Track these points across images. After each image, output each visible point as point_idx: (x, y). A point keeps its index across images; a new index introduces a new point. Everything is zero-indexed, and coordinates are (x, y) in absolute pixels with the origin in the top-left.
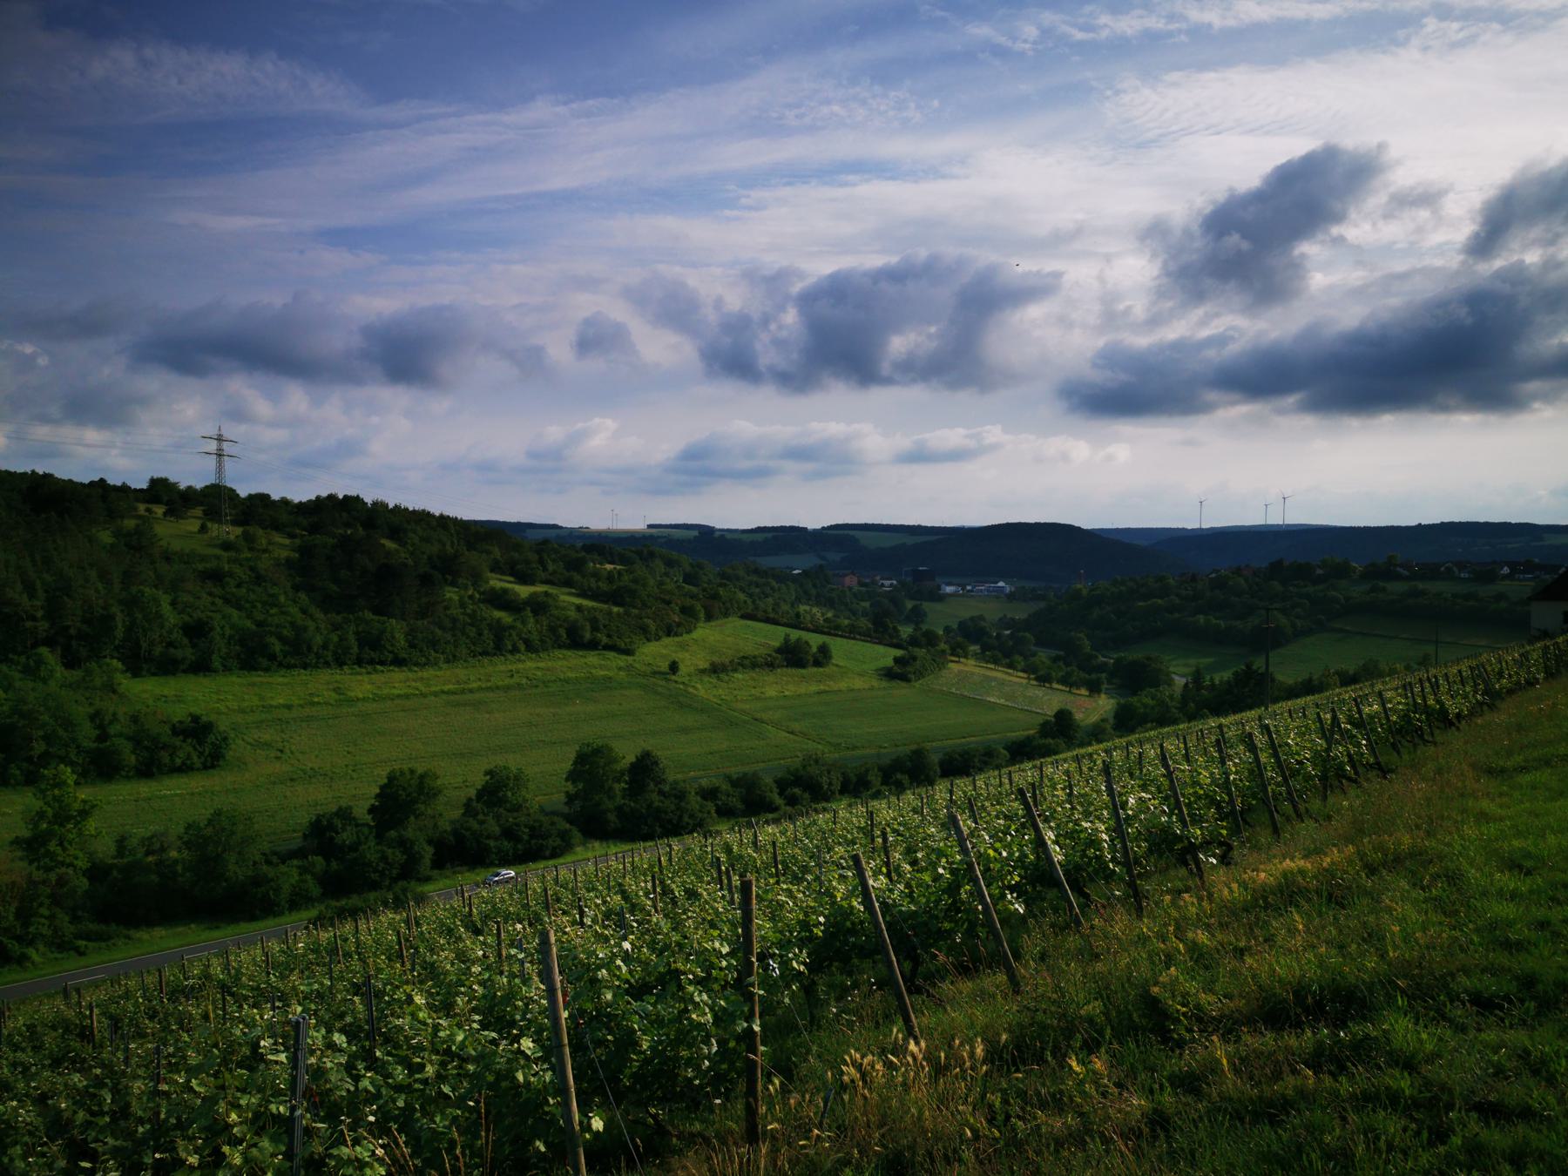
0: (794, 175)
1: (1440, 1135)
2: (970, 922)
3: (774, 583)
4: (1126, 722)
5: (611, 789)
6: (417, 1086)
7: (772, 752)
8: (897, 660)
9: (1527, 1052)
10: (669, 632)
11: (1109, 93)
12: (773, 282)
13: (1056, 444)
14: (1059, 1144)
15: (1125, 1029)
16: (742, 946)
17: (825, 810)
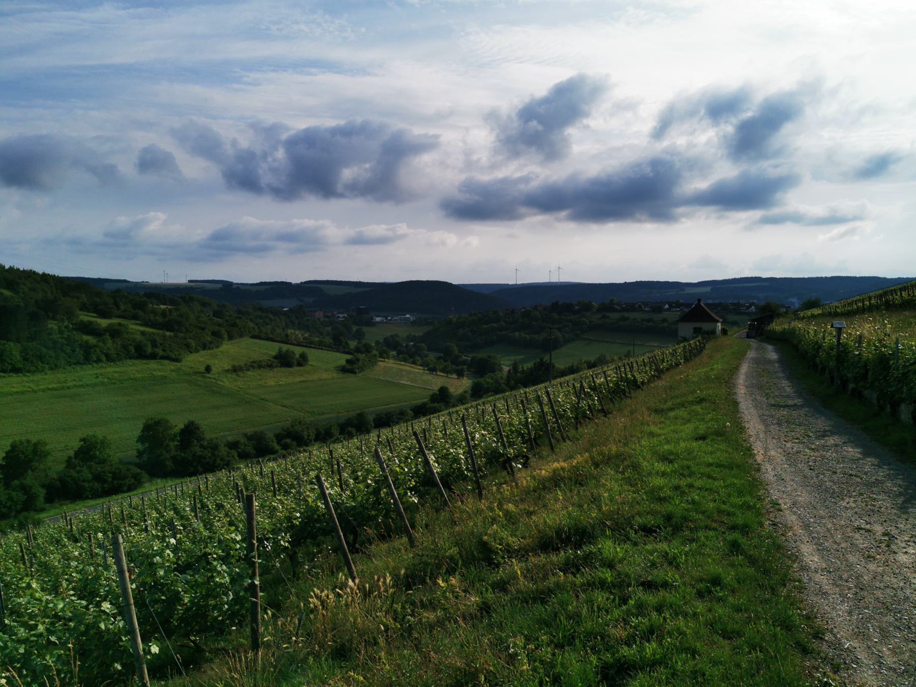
0: (279, 65)
1: (624, 601)
2: (387, 510)
3: (271, 316)
4: (477, 392)
5: (168, 445)
6: (33, 639)
7: (272, 419)
8: (348, 361)
9: (667, 553)
10: (204, 347)
11: (463, 34)
12: (270, 132)
13: (437, 236)
14: (432, 627)
15: (469, 560)
16: (248, 536)
17: (305, 451)
